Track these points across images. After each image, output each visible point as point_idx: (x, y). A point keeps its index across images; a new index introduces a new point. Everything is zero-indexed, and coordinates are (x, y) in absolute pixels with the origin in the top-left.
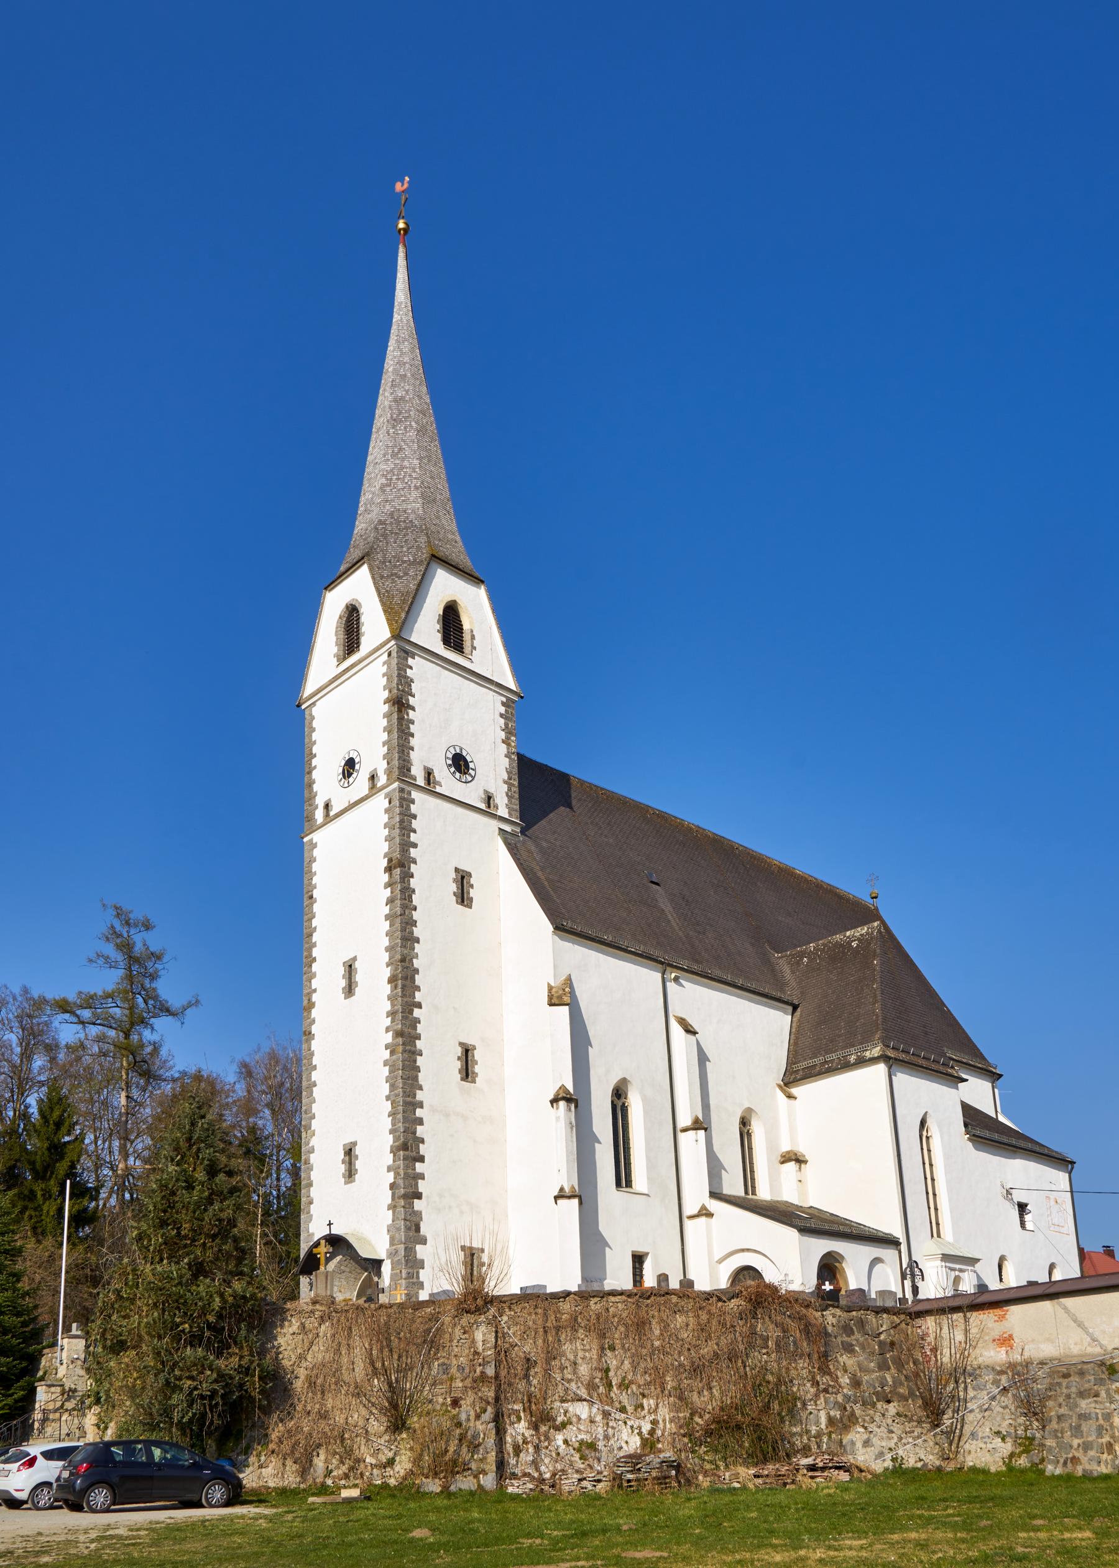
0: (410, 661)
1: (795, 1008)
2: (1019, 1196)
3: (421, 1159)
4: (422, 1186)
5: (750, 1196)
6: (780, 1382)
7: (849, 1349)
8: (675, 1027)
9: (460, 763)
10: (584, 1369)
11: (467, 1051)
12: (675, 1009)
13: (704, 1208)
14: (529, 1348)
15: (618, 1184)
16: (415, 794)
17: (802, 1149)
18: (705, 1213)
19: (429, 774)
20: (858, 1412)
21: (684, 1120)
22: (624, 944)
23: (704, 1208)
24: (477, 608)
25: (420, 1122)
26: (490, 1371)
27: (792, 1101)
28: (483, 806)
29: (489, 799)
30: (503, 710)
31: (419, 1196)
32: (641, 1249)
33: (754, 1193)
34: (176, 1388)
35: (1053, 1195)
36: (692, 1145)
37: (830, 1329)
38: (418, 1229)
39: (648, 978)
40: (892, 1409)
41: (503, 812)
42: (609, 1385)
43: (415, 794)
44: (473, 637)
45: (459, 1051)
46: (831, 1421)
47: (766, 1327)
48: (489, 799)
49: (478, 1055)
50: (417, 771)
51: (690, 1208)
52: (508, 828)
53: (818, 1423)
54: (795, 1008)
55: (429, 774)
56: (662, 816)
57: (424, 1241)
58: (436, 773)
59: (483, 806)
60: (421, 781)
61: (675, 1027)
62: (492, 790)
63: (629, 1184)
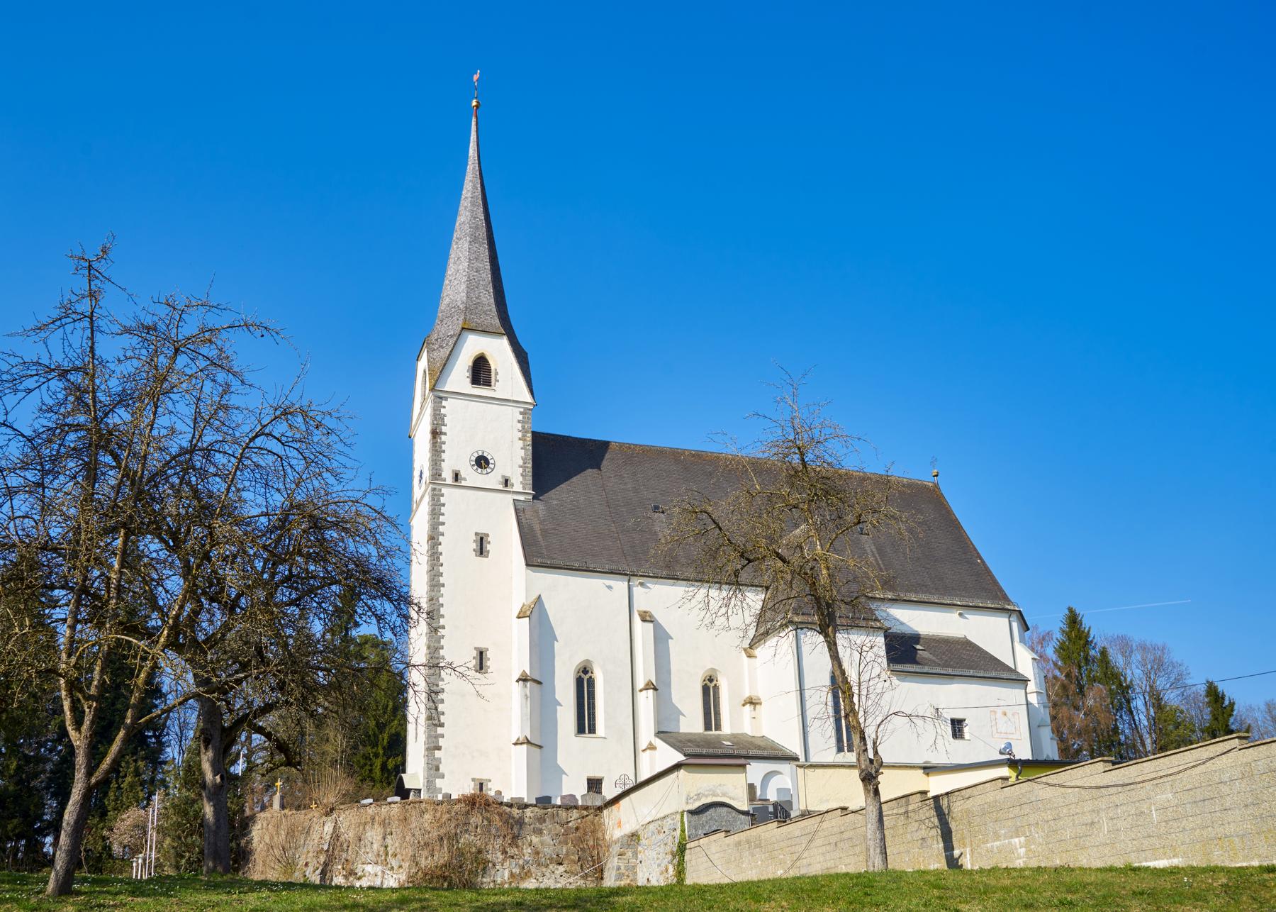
0: (444, 403)
1: (767, 588)
2: (949, 714)
3: (442, 725)
4: (441, 742)
5: (713, 732)
6: (480, 852)
7: (539, 832)
8: (637, 619)
9: (482, 462)
10: (375, 846)
11: (481, 653)
12: (639, 605)
13: (650, 744)
14: (351, 835)
15: (581, 730)
16: (444, 490)
17: (760, 693)
18: (652, 747)
19: (457, 477)
20: (533, 870)
21: (640, 684)
22: (592, 566)
23: (650, 744)
24: (499, 352)
25: (442, 701)
26: (326, 848)
27: (752, 660)
28: (501, 487)
29: (506, 482)
30: (520, 417)
31: (439, 748)
32: (597, 775)
33: (718, 727)
34: (183, 857)
35: (1000, 711)
36: (646, 701)
37: (527, 820)
38: (437, 769)
39: (620, 585)
40: (561, 869)
41: (518, 487)
42: (387, 854)
43: (444, 490)
44: (497, 374)
45: (475, 653)
46: (512, 875)
47: (476, 819)
48: (506, 482)
49: (489, 654)
50: (447, 476)
51: (643, 744)
52: (522, 498)
53: (502, 877)
54: (767, 588)
55: (457, 477)
56: (698, 456)
57: (443, 776)
58: (463, 474)
59: (501, 487)
60: (450, 480)
61: (637, 619)
62: (508, 474)
63: (592, 730)
